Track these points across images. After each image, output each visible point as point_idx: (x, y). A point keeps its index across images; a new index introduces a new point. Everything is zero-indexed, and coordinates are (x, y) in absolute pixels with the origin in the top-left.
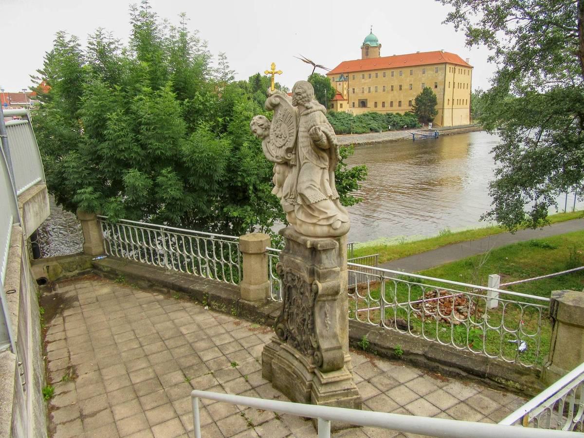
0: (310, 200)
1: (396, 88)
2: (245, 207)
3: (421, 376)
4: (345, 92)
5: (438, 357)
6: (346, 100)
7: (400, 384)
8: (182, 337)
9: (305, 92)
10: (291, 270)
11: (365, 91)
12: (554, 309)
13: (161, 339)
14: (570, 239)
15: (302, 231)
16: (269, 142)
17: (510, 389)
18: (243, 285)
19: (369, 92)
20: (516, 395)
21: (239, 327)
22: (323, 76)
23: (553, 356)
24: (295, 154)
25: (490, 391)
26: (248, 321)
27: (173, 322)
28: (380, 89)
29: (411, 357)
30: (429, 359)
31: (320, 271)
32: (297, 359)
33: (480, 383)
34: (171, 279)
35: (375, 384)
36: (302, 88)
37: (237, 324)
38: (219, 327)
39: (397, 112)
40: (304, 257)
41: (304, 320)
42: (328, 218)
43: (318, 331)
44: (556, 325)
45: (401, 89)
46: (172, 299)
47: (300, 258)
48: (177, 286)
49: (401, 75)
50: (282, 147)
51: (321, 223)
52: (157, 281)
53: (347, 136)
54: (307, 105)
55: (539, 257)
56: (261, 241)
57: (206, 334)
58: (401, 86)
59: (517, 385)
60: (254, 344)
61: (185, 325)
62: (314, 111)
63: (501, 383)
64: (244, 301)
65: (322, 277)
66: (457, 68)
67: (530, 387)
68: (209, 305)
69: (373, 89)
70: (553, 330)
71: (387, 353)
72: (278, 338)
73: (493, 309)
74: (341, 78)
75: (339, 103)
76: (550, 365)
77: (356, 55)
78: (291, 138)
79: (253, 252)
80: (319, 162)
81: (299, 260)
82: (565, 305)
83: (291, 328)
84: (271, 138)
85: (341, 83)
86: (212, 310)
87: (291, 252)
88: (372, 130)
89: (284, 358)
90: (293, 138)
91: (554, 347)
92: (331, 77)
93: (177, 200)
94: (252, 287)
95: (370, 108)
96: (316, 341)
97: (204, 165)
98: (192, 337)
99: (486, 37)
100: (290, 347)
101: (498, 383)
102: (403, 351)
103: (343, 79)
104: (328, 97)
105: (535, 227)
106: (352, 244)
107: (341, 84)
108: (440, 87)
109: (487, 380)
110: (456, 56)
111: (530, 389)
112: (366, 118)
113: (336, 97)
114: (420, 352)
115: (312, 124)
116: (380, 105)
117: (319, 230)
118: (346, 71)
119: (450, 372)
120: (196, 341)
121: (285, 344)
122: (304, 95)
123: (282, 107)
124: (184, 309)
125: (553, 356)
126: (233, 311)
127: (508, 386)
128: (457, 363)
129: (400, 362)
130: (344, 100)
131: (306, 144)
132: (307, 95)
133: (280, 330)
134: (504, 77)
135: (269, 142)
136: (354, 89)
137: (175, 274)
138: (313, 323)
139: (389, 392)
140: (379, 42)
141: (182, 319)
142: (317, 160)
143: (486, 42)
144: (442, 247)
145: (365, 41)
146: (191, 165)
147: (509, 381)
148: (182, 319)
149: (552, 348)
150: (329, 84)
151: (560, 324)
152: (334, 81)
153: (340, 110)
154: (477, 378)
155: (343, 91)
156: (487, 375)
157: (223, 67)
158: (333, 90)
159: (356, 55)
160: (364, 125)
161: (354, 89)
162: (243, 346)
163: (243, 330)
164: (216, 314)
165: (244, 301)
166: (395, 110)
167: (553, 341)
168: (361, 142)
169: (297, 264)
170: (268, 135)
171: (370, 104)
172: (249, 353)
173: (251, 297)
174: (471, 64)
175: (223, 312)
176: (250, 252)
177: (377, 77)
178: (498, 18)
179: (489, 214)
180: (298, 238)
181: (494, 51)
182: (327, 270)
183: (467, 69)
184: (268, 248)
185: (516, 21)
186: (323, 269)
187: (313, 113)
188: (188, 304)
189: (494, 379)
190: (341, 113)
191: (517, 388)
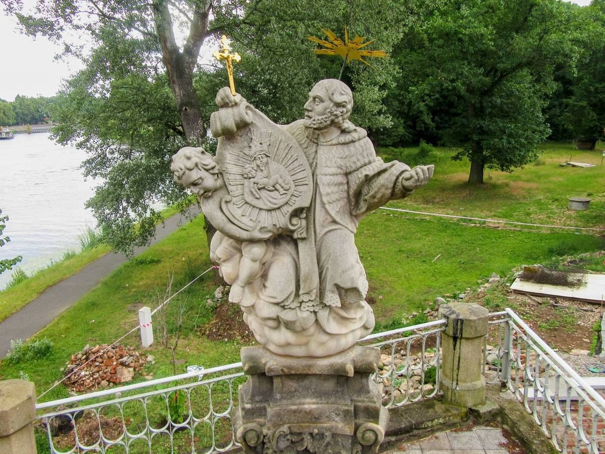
10: (289, 428)
14: (165, 249)
17: (435, 428)
20: (442, 431)
23: (457, 375)
44: (458, 343)
47: (308, 400)
50: (279, 208)
55: (153, 275)
70: (455, 349)
73: (151, 346)
76: (457, 384)
78: (301, 188)
81: (310, 404)
82: (470, 321)
90: (308, 191)
101: (425, 428)
109: (415, 432)
115: (367, 161)
125: (457, 375)
131: (335, 197)
143: (45, 33)
144: (41, 293)
147: (434, 420)
149: (455, 368)
169: (309, 413)
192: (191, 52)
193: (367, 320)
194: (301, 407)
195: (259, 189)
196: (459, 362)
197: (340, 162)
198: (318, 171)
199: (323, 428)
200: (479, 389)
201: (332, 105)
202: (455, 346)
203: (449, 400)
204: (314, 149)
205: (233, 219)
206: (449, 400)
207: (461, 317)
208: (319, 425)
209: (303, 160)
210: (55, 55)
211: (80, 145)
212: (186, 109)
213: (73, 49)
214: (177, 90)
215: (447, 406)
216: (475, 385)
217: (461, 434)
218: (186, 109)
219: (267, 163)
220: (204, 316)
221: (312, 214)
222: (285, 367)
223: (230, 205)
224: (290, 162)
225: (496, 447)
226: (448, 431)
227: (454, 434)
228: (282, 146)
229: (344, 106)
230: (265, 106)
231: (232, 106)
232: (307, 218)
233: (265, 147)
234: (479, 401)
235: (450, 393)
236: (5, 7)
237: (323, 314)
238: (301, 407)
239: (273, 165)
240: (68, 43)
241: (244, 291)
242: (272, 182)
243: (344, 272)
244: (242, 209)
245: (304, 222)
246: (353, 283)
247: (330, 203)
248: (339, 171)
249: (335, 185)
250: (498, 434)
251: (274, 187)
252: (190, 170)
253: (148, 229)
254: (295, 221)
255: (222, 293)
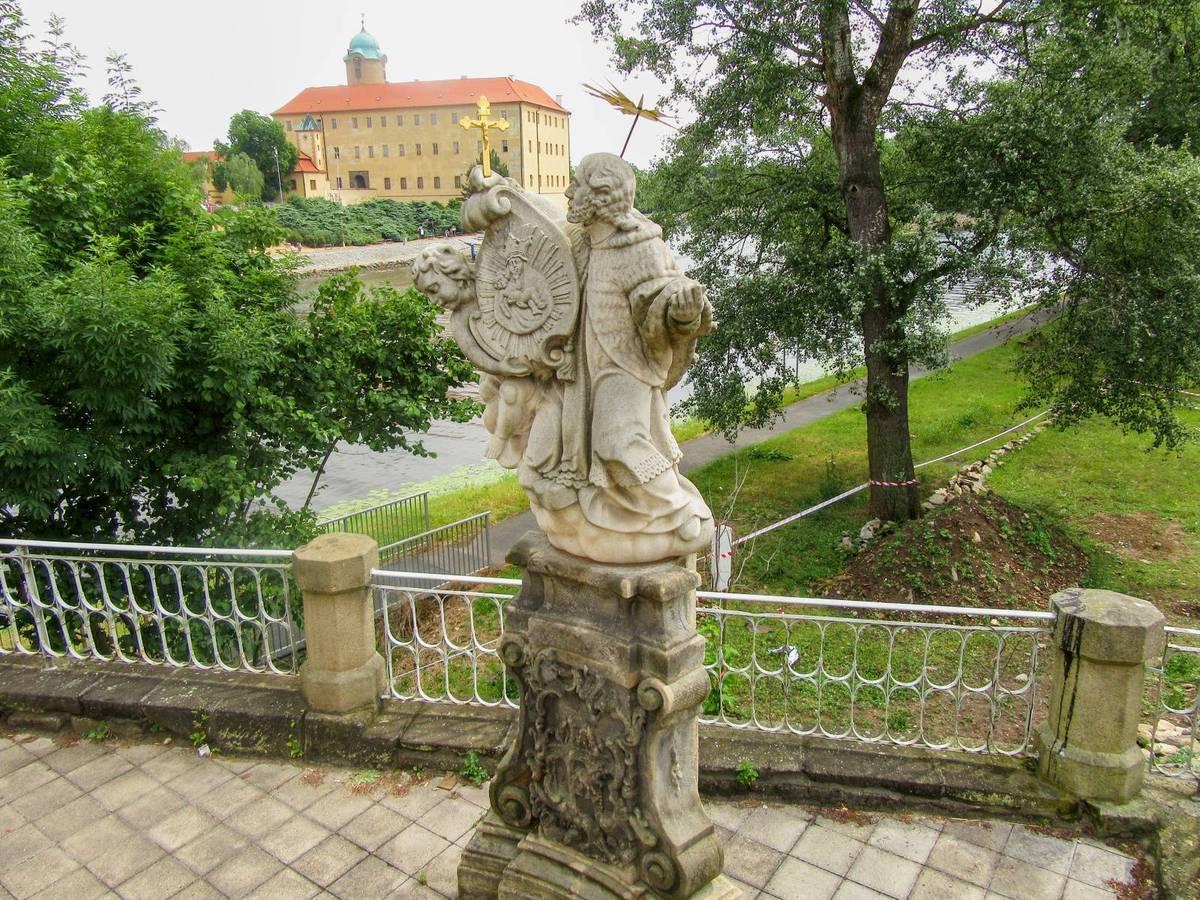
0: (637, 474)
1: (427, 149)
2: (223, 459)
3: (812, 822)
4: (319, 155)
5: (835, 771)
6: (323, 173)
7: (785, 857)
8: (168, 862)
9: (621, 185)
10: (554, 653)
11: (361, 155)
12: (1070, 637)
13: (106, 884)
15: (594, 555)
16: (476, 320)
18: (314, 675)
19: (371, 155)
20: (1006, 820)
21: (322, 790)
22: (266, 119)
23: (1067, 729)
24: (574, 351)
25: (962, 823)
26: (340, 766)
27: (119, 818)
28: (394, 151)
29: (776, 781)
30: (815, 778)
31: (666, 654)
32: (576, 873)
33: (930, 810)
34: (71, 684)
35: (733, 872)
36: (613, 175)
37: (311, 781)
38: (267, 802)
39: (433, 199)
40: (598, 618)
41: (606, 778)
42: (669, 517)
43: (657, 803)
45: (436, 152)
46: (84, 743)
47: (582, 621)
48: (97, 703)
49: (434, 123)
50: (531, 333)
51: (652, 529)
52: (24, 699)
53: (335, 251)
54: (620, 220)
55: (769, 478)
56: (360, 558)
57: (238, 834)
58: (435, 146)
59: (1008, 800)
60: (388, 833)
61: (160, 819)
62: (648, 239)
63: (974, 802)
64: (320, 716)
65: (663, 669)
66: (542, 113)
67: (1032, 800)
68: (210, 741)
69: (378, 150)
70: (1066, 677)
71: (720, 782)
72: (501, 824)
74: (306, 123)
75: (308, 178)
76: (1064, 746)
77: (336, 76)
78: (563, 308)
79: (340, 589)
80: (647, 372)
81: (582, 628)
82: (1098, 626)
83: (555, 799)
84: (485, 308)
85: (308, 134)
86: (225, 752)
87: (548, 606)
88: (387, 237)
89: (537, 878)
91: (1071, 710)
92: (283, 121)
93: (38, 457)
94: (342, 678)
95: (375, 192)
96: (648, 828)
97: (118, 354)
98: (203, 855)
99: (653, 56)
100: (548, 844)
101: (968, 802)
102: (758, 772)
103: (310, 126)
104: (281, 166)
105: (760, 423)
106: (425, 495)
107: (309, 137)
108: (513, 150)
109: (945, 802)
110: (538, 89)
111: (1033, 804)
112: (372, 212)
113: (301, 166)
114: (795, 767)
115: (645, 275)
116: (396, 185)
117: (646, 548)
118: (315, 109)
119: (867, 799)
120: (220, 865)
121: (530, 838)
122: (618, 193)
123: (520, 221)
124: (137, 768)
126: (291, 748)
127: (987, 804)
128: (880, 776)
129: (752, 796)
130: (318, 172)
131: (613, 325)
132: (626, 194)
133: (511, 805)
134: (701, 136)
135: (476, 320)
136: (337, 149)
137: (76, 666)
138: (640, 784)
139: (774, 883)
140: (382, 52)
141: (144, 802)
142: (642, 369)
143: (652, 67)
145: (353, 45)
146: (78, 357)
148: (144, 802)
149: (1065, 713)
150: (282, 137)
151: (1085, 663)
152: (290, 129)
153: (310, 194)
154: (922, 800)
155: (314, 152)
156: (943, 790)
157: (121, 92)
158: (292, 151)
159: (336, 76)
160: (368, 227)
161: (337, 149)
162: (362, 849)
163: (338, 795)
164: (241, 765)
165: (320, 716)
166: (428, 195)
167: (1068, 699)
168: (366, 264)
169: (578, 639)
170: (473, 299)
171: (376, 181)
172: (389, 865)
173: (344, 700)
174: (566, 107)
175: (260, 755)
176: (334, 589)
177: (384, 125)
178: (679, 22)
179: (685, 405)
180: (580, 571)
181: (671, 85)
182: (681, 647)
183: (560, 117)
184: (375, 572)
185: (711, 29)
186: (671, 647)
187: (647, 244)
188: (142, 751)
189: (959, 796)
190: (315, 202)
191: (1006, 806)
192: (876, 83)
193: (683, 525)
194: (569, 628)
195: (510, 305)
196: (1073, 702)
197: (613, 274)
198: (588, 287)
199: (594, 665)
200: (1110, 769)
201: (589, 190)
202: (1067, 670)
203: (1044, 771)
204: (586, 255)
205: (484, 347)
206: (1044, 771)
207: (1081, 615)
208: (591, 661)
209: (570, 268)
210: (658, 99)
211: (685, 248)
212: (854, 189)
213: (688, 87)
214: (843, 153)
215: (1035, 781)
216: (1103, 758)
217: (1041, 838)
218: (854, 189)
219: (522, 270)
220: (829, 565)
221: (580, 346)
222: (550, 563)
223: (480, 324)
224: (553, 270)
225: (1099, 882)
226: (1018, 826)
227: (1027, 834)
228: (547, 247)
229: (606, 193)
230: (1012, 183)
231: (482, 191)
232: (574, 351)
233: (522, 248)
234: (1107, 792)
235: (1046, 758)
236: (593, 29)
237: (586, 496)
238: (569, 628)
239: (531, 273)
240: (681, 78)
241: (504, 448)
242: (524, 295)
243: (605, 434)
244: (493, 330)
245: (569, 358)
246: (613, 452)
247: (604, 334)
248: (614, 288)
249: (611, 308)
250: (1123, 867)
251: (526, 303)
252: (424, 272)
253: (768, 404)
254: (553, 355)
255: (875, 530)
